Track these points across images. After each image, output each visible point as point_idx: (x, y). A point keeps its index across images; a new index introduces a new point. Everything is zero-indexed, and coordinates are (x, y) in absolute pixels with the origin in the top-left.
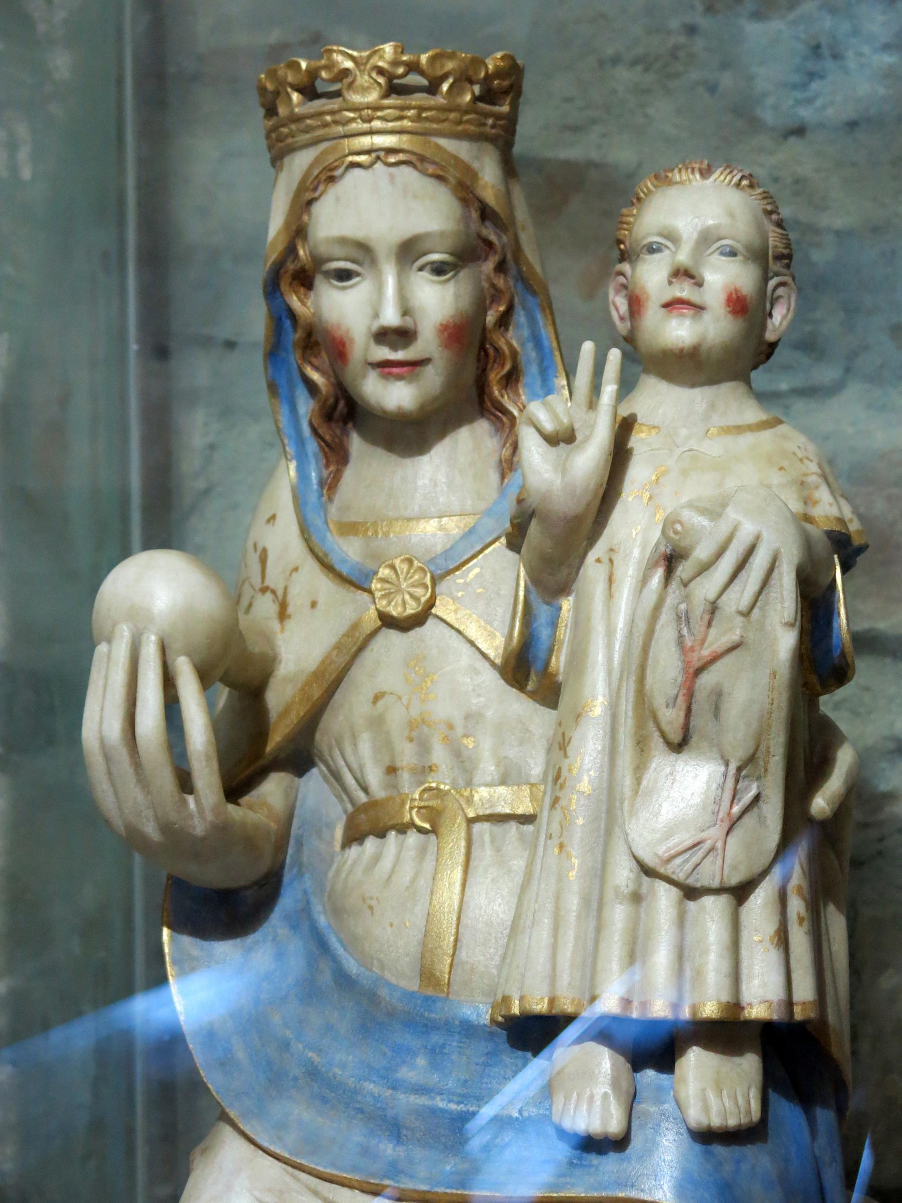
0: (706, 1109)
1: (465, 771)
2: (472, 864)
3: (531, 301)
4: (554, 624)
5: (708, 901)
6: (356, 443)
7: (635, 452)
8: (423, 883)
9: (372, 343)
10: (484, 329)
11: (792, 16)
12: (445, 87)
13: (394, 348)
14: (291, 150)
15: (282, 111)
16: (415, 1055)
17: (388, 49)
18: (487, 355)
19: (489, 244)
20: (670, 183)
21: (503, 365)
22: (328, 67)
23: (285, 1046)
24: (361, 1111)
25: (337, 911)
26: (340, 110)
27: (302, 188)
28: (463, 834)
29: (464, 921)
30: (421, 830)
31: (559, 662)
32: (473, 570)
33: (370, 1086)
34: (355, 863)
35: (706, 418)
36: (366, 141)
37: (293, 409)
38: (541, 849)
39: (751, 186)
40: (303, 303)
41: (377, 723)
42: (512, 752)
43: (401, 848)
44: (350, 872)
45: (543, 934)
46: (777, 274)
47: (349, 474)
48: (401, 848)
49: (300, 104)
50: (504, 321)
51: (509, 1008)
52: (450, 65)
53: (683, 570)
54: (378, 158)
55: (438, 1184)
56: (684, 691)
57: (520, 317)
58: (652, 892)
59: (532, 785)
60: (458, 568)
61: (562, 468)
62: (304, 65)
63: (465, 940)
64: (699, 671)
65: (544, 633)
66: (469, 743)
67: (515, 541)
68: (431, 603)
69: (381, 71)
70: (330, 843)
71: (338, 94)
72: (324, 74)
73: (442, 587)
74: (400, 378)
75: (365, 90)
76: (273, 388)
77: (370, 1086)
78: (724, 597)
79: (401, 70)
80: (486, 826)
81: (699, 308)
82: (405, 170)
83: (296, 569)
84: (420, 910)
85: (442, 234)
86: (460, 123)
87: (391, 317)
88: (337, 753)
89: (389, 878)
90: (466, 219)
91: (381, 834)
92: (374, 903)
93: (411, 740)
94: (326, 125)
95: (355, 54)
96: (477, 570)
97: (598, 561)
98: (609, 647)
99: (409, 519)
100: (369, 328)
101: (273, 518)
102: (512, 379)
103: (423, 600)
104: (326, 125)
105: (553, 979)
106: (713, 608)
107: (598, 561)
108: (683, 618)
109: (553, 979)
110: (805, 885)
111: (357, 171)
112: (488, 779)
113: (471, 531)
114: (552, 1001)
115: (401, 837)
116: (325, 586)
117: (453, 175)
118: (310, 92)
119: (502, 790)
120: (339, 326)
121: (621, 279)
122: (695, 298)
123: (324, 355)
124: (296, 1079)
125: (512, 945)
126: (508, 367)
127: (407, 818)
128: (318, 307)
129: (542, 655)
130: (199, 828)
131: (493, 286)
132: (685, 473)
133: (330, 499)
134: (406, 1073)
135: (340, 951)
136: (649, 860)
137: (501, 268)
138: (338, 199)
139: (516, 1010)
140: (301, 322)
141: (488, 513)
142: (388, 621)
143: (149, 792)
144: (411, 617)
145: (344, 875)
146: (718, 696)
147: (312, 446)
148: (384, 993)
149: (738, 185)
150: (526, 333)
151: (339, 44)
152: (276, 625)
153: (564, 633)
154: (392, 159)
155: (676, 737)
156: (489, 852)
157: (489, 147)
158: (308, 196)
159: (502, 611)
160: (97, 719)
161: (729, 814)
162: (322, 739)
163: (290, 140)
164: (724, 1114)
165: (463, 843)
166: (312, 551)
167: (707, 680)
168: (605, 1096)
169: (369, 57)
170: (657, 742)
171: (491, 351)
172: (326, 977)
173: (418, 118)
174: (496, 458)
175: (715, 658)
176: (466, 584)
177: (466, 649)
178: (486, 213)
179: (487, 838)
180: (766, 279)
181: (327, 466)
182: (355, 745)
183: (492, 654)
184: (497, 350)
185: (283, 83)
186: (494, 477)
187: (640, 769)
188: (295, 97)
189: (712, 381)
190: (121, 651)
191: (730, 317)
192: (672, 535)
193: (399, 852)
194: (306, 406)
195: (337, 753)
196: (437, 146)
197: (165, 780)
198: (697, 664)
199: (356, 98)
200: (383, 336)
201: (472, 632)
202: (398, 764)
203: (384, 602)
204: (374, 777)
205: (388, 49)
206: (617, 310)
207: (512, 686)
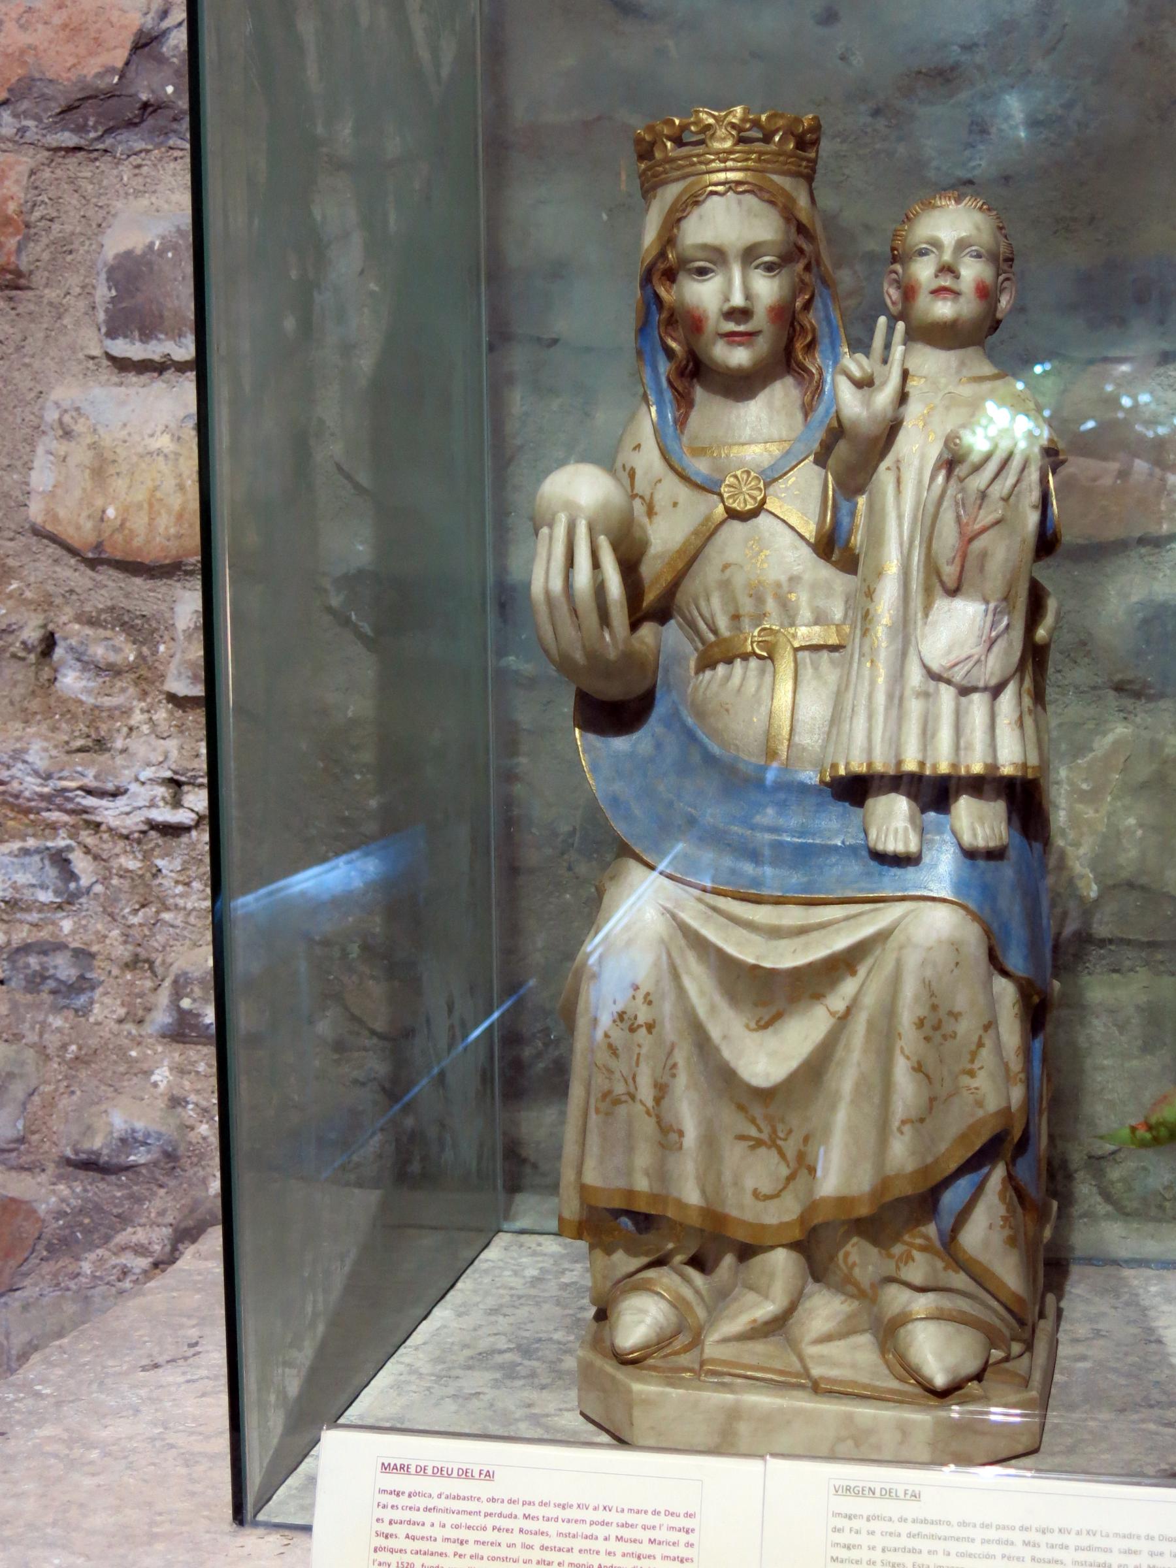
0: (975, 835)
1: (789, 617)
2: (799, 678)
3: (825, 292)
4: (853, 514)
5: (976, 697)
6: (699, 393)
7: (911, 395)
8: (765, 692)
9: (722, 320)
10: (794, 312)
11: (952, 102)
12: (777, 138)
13: (738, 323)
14: (664, 183)
15: (658, 155)
16: (765, 807)
17: (739, 110)
18: (794, 330)
19: (801, 251)
20: (935, 207)
21: (805, 338)
22: (694, 123)
23: (670, 804)
24: (729, 845)
25: (700, 714)
26: (703, 155)
27: (673, 209)
28: (792, 658)
29: (796, 717)
30: (760, 657)
31: (858, 539)
32: (792, 478)
33: (735, 828)
34: (709, 682)
35: (958, 371)
36: (722, 176)
37: (655, 369)
38: (855, 665)
39: (989, 210)
40: (667, 291)
41: (725, 585)
42: (821, 603)
43: (746, 669)
44: (706, 689)
45: (860, 723)
46: (1005, 272)
47: (694, 416)
48: (746, 669)
49: (673, 150)
50: (807, 306)
51: (837, 771)
52: (781, 123)
53: (960, 471)
54: (730, 188)
55: (787, 891)
56: (960, 554)
57: (818, 303)
58: (937, 690)
59: (837, 626)
60: (781, 477)
61: (867, 403)
62: (677, 122)
63: (799, 728)
64: (971, 540)
65: (845, 521)
66: (793, 597)
67: (821, 460)
68: (763, 502)
69: (733, 126)
70: (688, 670)
71: (702, 142)
72: (693, 128)
73: (771, 489)
74: (740, 344)
75: (724, 139)
76: (640, 353)
77: (735, 828)
78: (991, 489)
79: (748, 126)
80: (806, 654)
81: (956, 294)
82: (749, 198)
83: (660, 481)
84: (764, 710)
85: (773, 242)
86: (786, 163)
87: (738, 300)
88: (693, 607)
89: (739, 690)
90: (787, 232)
91: (729, 661)
92: (729, 706)
93: (751, 596)
94: (693, 164)
95: (716, 113)
96: (793, 479)
97: (888, 469)
98: (900, 525)
99: (743, 444)
100: (721, 310)
101: (638, 447)
102: (810, 347)
103: (759, 498)
104: (693, 164)
105: (870, 750)
106: (983, 495)
107: (888, 469)
108: (960, 504)
109: (870, 750)
110: (1032, 689)
111: (715, 198)
112: (806, 621)
113: (788, 453)
114: (870, 765)
115: (744, 663)
116: (683, 492)
117: (781, 200)
118: (679, 142)
119: (817, 628)
120: (698, 308)
121: (894, 276)
122: (955, 287)
123: (681, 330)
124: (679, 826)
125: (834, 731)
126: (809, 338)
127: (749, 649)
128: (680, 293)
129: (844, 536)
130: (612, 654)
131: (802, 281)
132: (948, 408)
133: (682, 432)
134: (758, 819)
135: (706, 740)
136: (935, 667)
137: (808, 268)
138: (701, 217)
139: (842, 771)
140: (666, 305)
141: (798, 440)
142: (733, 514)
143: (579, 628)
144: (750, 510)
145: (701, 690)
146: (984, 555)
147: (668, 395)
148: (741, 766)
149: (981, 208)
150: (822, 314)
151: (704, 107)
152: (645, 520)
153: (861, 520)
154: (740, 189)
155: (951, 583)
156: (810, 671)
157: (802, 181)
158: (679, 215)
159: (814, 507)
160: (542, 580)
161: (989, 637)
162: (681, 598)
163: (663, 176)
164: (986, 838)
165: (792, 665)
166: (672, 468)
167: (977, 545)
168: (906, 829)
169: (726, 116)
170: (938, 590)
171: (798, 328)
172: (696, 758)
173: (759, 160)
174: (799, 402)
175: (984, 530)
176: (787, 489)
177: (788, 531)
178: (801, 229)
179: (808, 660)
180: (998, 275)
181: (679, 409)
182: (708, 600)
183: (807, 536)
184: (802, 327)
185: (662, 134)
186: (799, 416)
187: (927, 609)
188: (669, 144)
189: (962, 345)
190: (560, 531)
191: (978, 300)
192: (952, 446)
193: (745, 673)
194: (664, 367)
195: (693, 607)
196: (772, 180)
197: (591, 618)
198: (970, 534)
199: (717, 145)
200: (733, 314)
201: (793, 521)
202: (741, 612)
203: (731, 501)
204: (723, 623)
205: (739, 110)
206: (890, 297)
207: (821, 558)
